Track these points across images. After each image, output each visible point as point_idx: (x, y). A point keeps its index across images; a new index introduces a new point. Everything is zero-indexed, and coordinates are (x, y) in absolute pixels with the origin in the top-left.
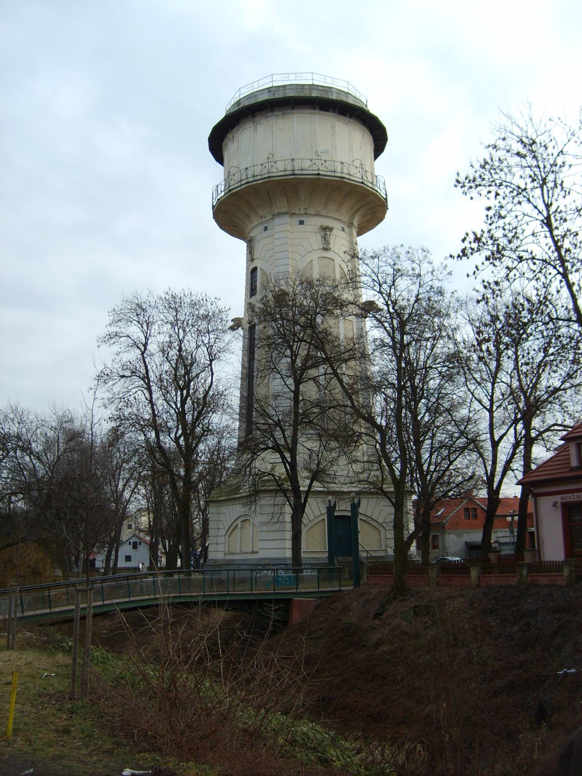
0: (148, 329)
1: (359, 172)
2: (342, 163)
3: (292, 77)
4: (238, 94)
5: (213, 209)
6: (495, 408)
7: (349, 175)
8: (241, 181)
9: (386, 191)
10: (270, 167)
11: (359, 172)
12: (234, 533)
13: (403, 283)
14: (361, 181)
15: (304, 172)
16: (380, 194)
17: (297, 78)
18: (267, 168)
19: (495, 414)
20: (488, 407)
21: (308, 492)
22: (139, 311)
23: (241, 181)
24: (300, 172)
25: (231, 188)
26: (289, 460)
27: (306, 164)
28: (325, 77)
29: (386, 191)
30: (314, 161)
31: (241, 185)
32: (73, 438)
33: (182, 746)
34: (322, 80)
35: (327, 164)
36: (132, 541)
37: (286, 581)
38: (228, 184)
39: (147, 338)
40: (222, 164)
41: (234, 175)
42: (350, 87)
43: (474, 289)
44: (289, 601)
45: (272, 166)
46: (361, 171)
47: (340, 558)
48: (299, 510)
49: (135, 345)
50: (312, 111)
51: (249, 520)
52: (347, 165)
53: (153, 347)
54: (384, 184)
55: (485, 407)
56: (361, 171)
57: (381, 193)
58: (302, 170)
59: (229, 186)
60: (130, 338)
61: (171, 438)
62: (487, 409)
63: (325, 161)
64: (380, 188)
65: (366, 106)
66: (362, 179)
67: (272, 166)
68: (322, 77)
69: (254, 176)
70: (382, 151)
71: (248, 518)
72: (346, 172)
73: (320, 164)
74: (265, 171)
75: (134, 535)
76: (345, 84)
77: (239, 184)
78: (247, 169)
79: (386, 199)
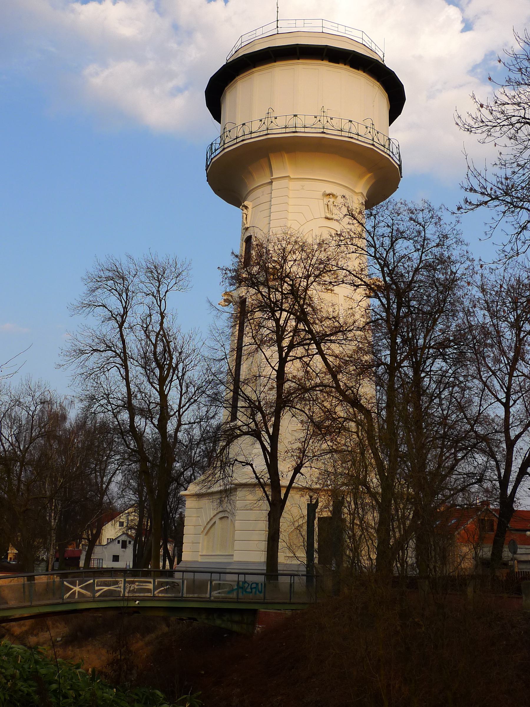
0: (127, 298)
1: (370, 132)
2: (350, 121)
3: (300, 23)
4: (239, 42)
5: (206, 170)
6: (511, 403)
8: (237, 138)
9: (399, 156)
10: (270, 122)
11: (370, 132)
12: (211, 531)
13: (403, 247)
14: (371, 142)
15: (307, 130)
16: (392, 158)
17: (305, 25)
18: (266, 123)
19: (512, 410)
20: (504, 401)
21: (289, 488)
22: (117, 279)
23: (237, 138)
24: (303, 130)
25: (226, 146)
26: (269, 449)
27: (310, 121)
29: (399, 156)
30: (318, 118)
31: (237, 143)
32: (51, 420)
34: (333, 28)
35: (334, 122)
36: (120, 539)
37: (251, 589)
38: (222, 142)
39: (125, 313)
40: (220, 123)
41: (230, 131)
42: (365, 38)
44: (254, 612)
45: (272, 122)
46: (371, 131)
48: (277, 507)
49: (113, 317)
51: (228, 517)
52: (356, 125)
53: (132, 318)
54: (398, 148)
55: (499, 400)
57: (394, 158)
59: (224, 144)
60: (106, 307)
61: (154, 424)
62: (502, 403)
63: (331, 119)
64: (392, 153)
65: (383, 61)
66: (373, 140)
70: (399, 113)
71: (226, 515)
74: (264, 127)
75: (124, 533)
76: (360, 34)
77: (235, 141)
78: (244, 124)
79: (400, 166)
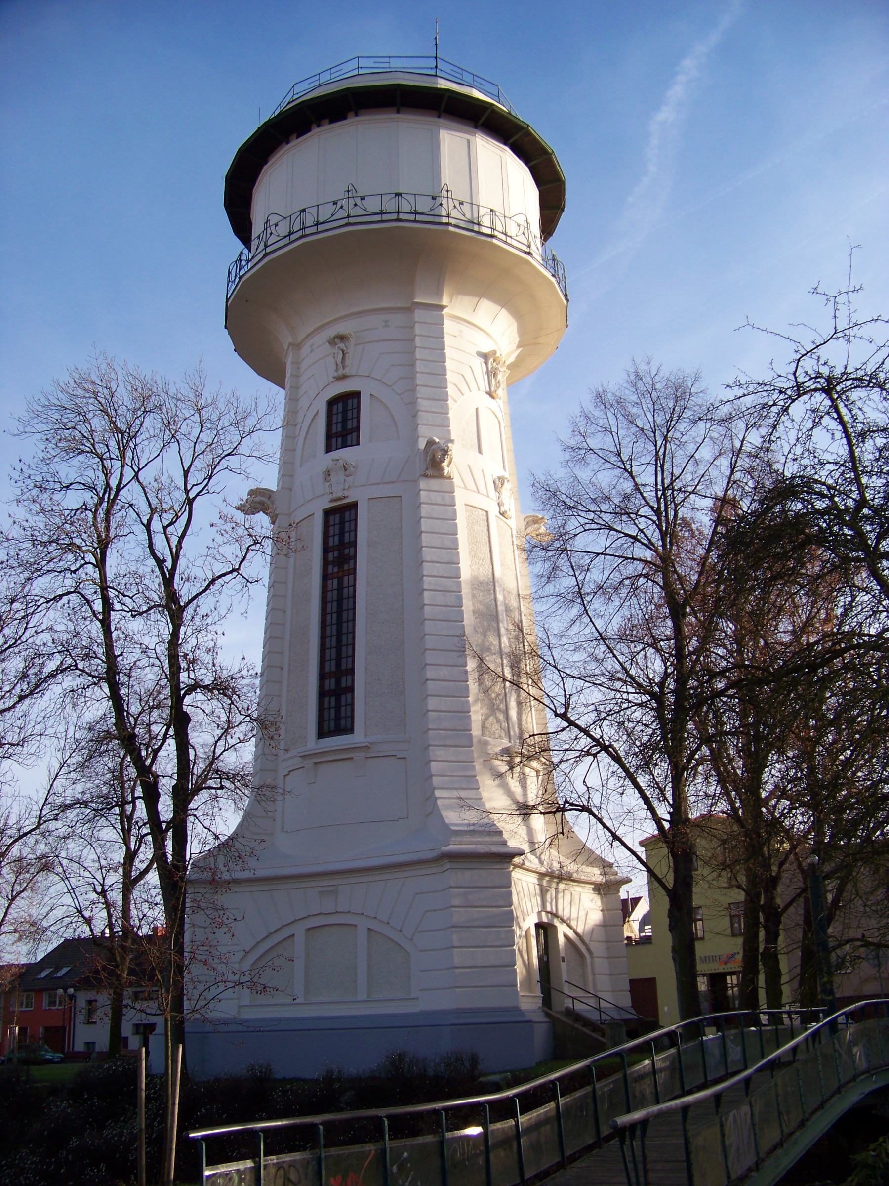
1: (524, 234)
7: (506, 235)
8: (290, 234)
11: (524, 234)
23: (290, 234)
28: (460, 71)
33: (879, 929)
41: (276, 225)
43: (417, 998)
47: (373, 1152)
50: (436, 119)
56: (526, 231)
58: (415, 213)
59: (266, 246)
66: (529, 246)
67: (356, 205)
68: (456, 69)
69: (317, 224)
70: (551, 235)
72: (499, 227)
73: (451, 207)
78: (303, 211)
